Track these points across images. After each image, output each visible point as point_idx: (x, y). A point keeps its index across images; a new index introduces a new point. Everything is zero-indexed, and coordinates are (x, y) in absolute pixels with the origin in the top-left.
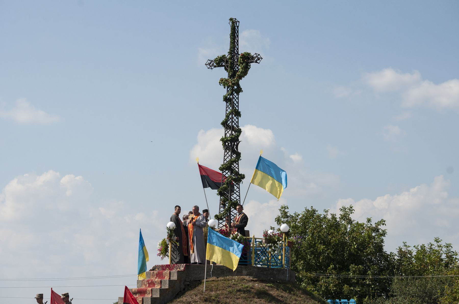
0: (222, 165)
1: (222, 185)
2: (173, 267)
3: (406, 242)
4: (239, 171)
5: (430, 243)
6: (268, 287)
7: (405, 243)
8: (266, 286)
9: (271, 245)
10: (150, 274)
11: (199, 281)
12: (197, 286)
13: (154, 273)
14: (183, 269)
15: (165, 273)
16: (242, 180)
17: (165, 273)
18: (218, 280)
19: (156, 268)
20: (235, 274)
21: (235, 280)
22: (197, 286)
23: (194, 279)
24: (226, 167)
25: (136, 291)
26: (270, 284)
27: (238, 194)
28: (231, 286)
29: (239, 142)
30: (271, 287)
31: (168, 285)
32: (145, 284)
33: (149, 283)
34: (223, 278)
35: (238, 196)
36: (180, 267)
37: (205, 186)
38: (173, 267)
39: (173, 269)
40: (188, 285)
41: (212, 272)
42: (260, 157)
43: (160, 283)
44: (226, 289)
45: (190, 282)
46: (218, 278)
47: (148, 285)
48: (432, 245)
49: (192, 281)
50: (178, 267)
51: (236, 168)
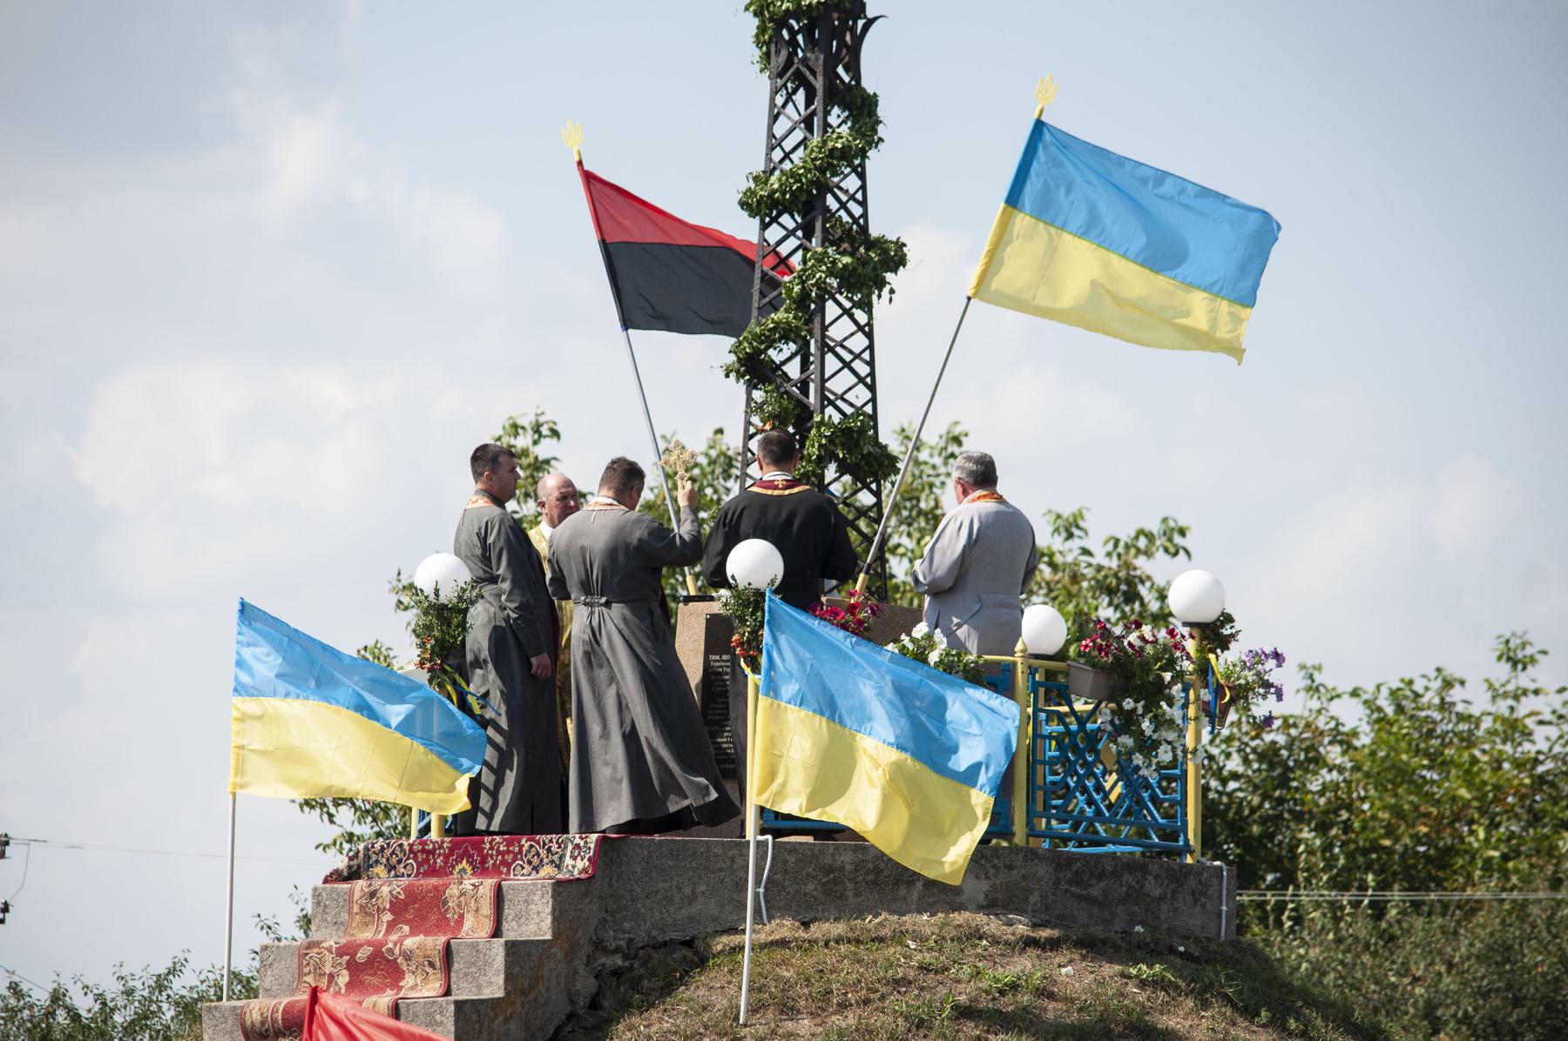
0: (756, 179)
1: (759, 308)
2: (509, 858)
3: (1319, 668)
4: (865, 215)
5: (1439, 670)
6: (1143, 984)
7: (1316, 675)
8: (1129, 977)
9: (1135, 709)
10: (350, 901)
11: (689, 944)
12: (682, 977)
13: (373, 894)
14: (584, 870)
15: (462, 894)
16: (889, 276)
17: (462, 894)
18: (812, 942)
19: (377, 862)
20: (915, 897)
21: (921, 939)
22: (682, 977)
23: (655, 933)
24: (793, 193)
25: (274, 1021)
26: (1150, 966)
27: (863, 370)
28: (910, 983)
29: (870, 22)
30: (1157, 984)
31: (502, 976)
32: (328, 969)
33: (353, 967)
34: (839, 929)
35: (861, 380)
36: (561, 858)
37: (627, 323)
38: (508, 852)
39: (508, 865)
40: (617, 973)
41: (767, 882)
42: (1039, 125)
43: (438, 964)
44: (883, 998)
45: (626, 957)
46: (806, 925)
47: (347, 979)
48: (1448, 684)
49: (642, 948)
50: (543, 853)
51: (852, 198)
